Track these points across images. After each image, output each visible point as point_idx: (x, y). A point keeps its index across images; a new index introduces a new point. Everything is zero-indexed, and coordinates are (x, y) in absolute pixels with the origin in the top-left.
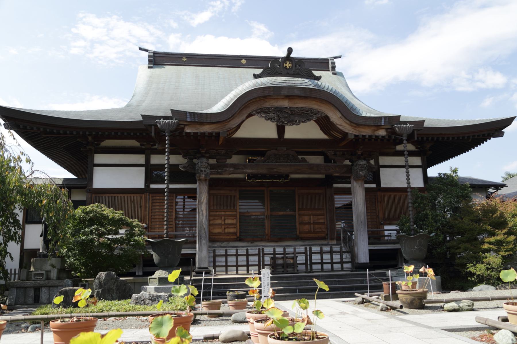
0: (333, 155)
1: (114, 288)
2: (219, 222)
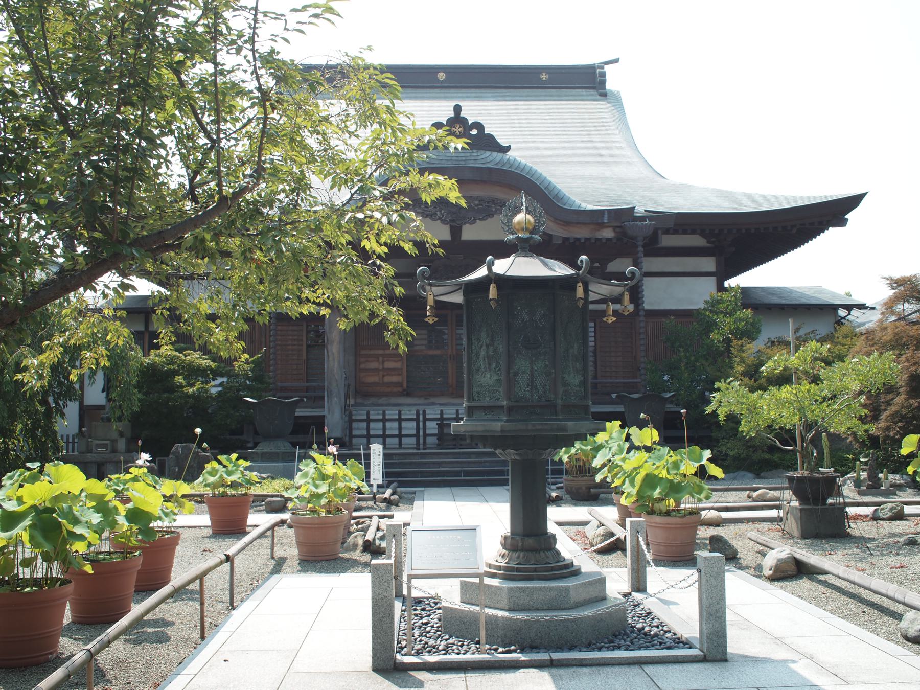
2: (374, 365)
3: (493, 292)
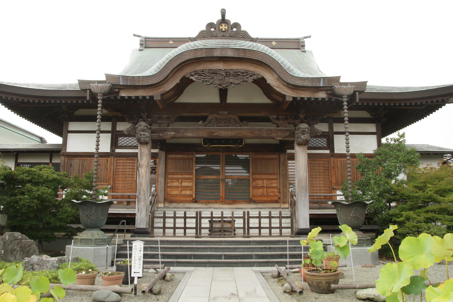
0: (276, 119)
1: (18, 249)
2: (176, 184)
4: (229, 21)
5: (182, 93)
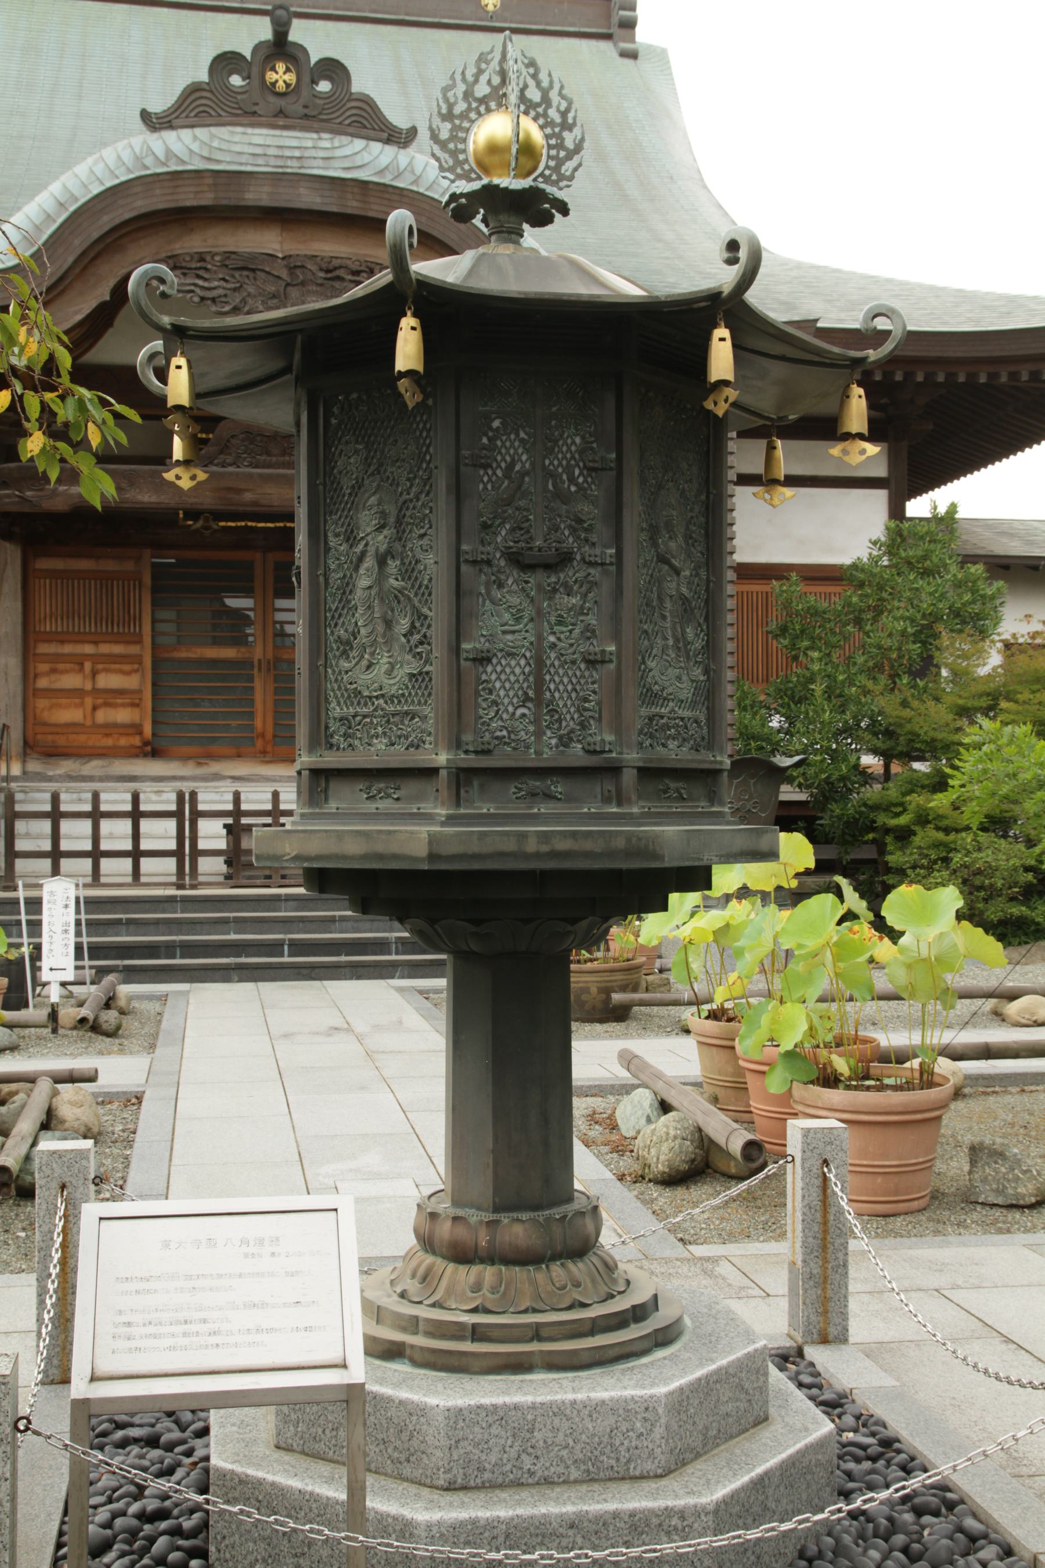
2: (71, 681)
3: (408, 348)
4: (304, 51)
5: (111, 325)
